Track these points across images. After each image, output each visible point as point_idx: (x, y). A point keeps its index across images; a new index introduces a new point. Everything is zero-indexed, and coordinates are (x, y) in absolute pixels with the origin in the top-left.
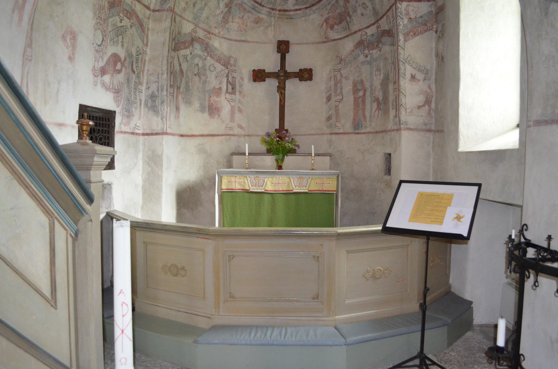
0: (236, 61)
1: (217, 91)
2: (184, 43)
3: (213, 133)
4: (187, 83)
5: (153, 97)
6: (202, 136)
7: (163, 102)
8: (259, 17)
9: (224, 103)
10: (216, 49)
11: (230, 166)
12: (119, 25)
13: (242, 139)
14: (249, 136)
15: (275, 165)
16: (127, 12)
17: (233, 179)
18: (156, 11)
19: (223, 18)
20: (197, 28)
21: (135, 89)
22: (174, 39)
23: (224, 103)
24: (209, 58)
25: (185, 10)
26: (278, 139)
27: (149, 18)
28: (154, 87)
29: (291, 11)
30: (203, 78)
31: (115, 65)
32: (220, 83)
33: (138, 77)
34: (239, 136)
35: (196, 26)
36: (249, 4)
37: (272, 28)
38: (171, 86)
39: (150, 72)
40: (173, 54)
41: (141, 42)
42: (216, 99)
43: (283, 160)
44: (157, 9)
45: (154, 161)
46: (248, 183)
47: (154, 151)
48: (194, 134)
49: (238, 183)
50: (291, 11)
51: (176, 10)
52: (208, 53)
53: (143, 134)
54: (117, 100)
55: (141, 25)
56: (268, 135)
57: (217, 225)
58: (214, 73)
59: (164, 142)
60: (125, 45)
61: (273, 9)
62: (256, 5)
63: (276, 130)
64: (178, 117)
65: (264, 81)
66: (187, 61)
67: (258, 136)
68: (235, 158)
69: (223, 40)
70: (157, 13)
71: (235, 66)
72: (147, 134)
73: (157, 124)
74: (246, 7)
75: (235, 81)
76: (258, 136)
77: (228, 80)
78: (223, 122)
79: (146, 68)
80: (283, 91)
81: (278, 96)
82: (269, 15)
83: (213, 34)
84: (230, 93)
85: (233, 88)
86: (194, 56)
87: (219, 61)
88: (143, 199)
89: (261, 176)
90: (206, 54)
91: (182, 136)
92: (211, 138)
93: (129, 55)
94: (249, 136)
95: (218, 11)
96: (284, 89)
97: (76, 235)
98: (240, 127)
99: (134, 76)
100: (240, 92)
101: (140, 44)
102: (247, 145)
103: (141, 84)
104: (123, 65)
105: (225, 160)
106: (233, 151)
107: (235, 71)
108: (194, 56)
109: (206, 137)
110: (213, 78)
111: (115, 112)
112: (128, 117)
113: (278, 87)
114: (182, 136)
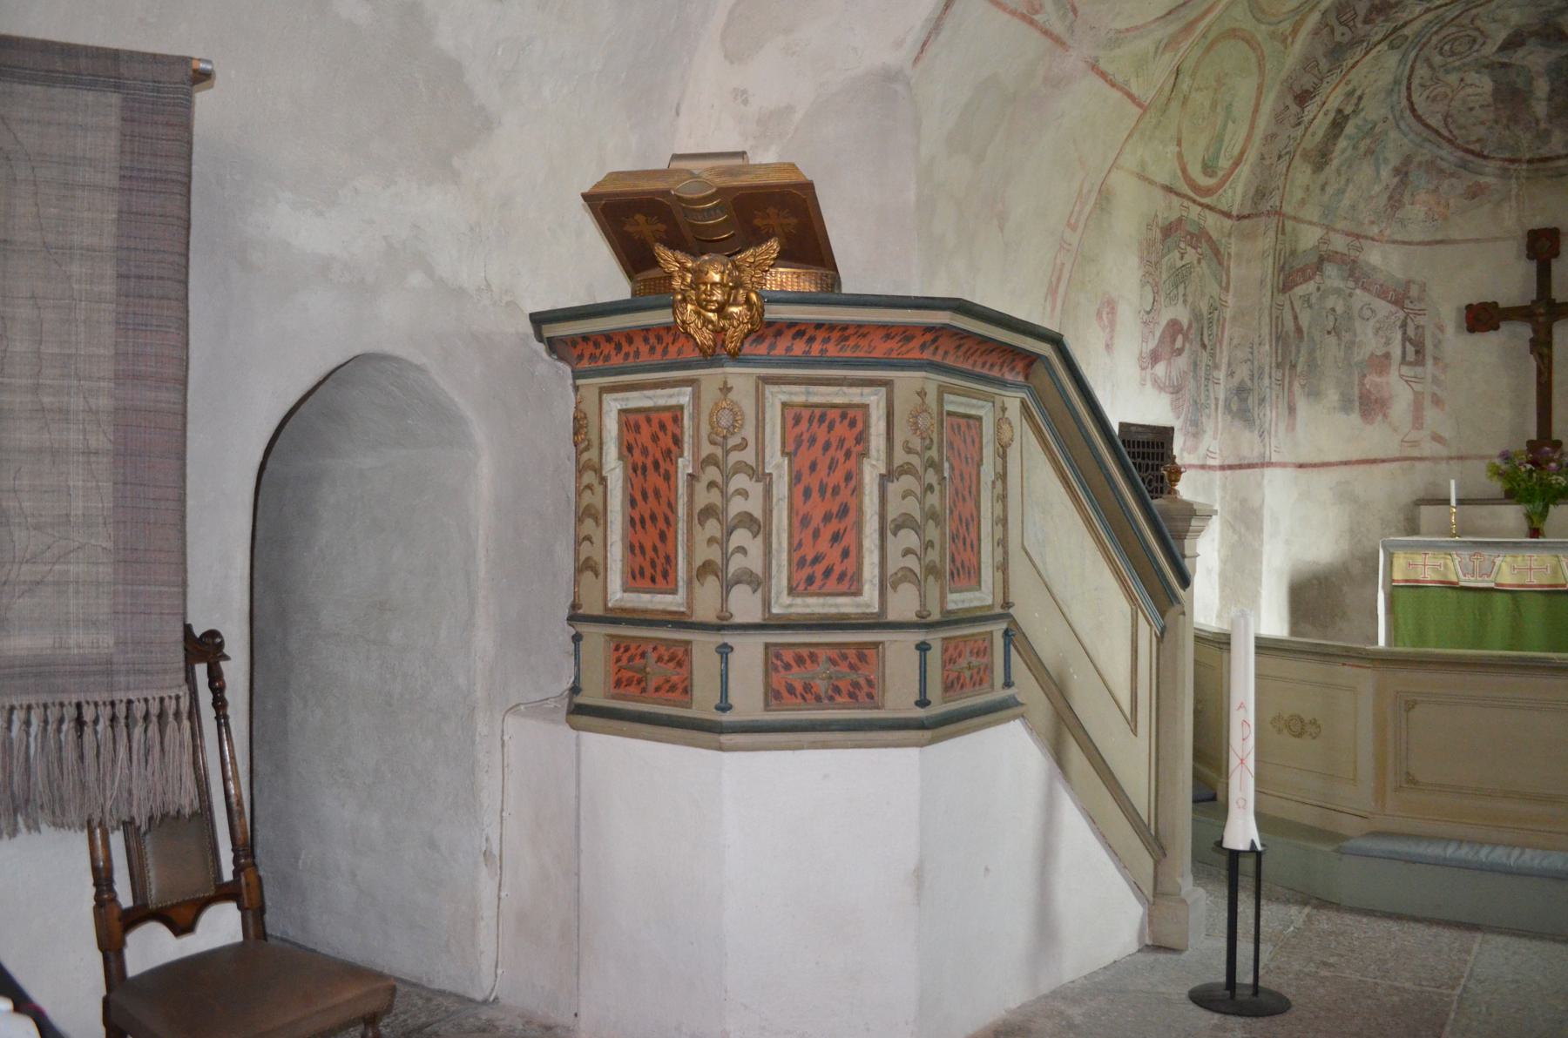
0: (1423, 288)
1: (1381, 363)
2: (1303, 270)
3: (1372, 457)
4: (1311, 352)
5: (1241, 391)
6: (1346, 463)
7: (1262, 401)
8: (1478, 184)
9: (1401, 395)
10: (1374, 268)
11: (1413, 529)
12: (1179, 264)
13: (1443, 466)
14: (1461, 458)
15: (1525, 527)
16: (1192, 235)
17: (1419, 559)
18: (1244, 217)
19: (1390, 198)
20: (1331, 234)
21: (1207, 379)
22: (1282, 268)
23: (1398, 388)
24: (1358, 291)
25: (1303, 202)
26: (1529, 466)
27: (1229, 235)
28: (1243, 372)
29: (1559, 157)
30: (1346, 337)
31: (1174, 341)
32: (1387, 343)
33: (1213, 355)
34: (1434, 459)
35: (1329, 228)
36: (1452, 159)
37: (1514, 203)
38: (1278, 366)
39: (1235, 342)
40: (1281, 298)
41: (1216, 286)
42: (1378, 379)
43: (1544, 514)
44: (1246, 212)
45: (1246, 520)
46: (1456, 567)
47: (1243, 501)
48: (1326, 459)
49: (1429, 567)
50: (1559, 157)
51: (1288, 209)
52: (1356, 281)
53: (1222, 468)
54: (1176, 408)
55: (1217, 252)
56: (1506, 456)
57: (1382, 642)
58: (1372, 322)
59: (1266, 482)
60: (1190, 299)
61: (1512, 161)
62: (1470, 157)
63: (1530, 443)
64: (1293, 429)
65: (1496, 328)
66: (1310, 306)
67: (1482, 457)
68: (1426, 512)
69: (1389, 248)
70: (1246, 222)
71: (1420, 300)
72: (1231, 467)
73: (1249, 445)
74: (1444, 165)
75: (1423, 335)
76: (1482, 457)
77: (1405, 333)
78: (1395, 430)
79: (1226, 335)
80: (1546, 351)
81: (1532, 363)
82: (1504, 174)
83: (1366, 237)
84: (1410, 364)
85: (1417, 350)
86: (1323, 293)
87: (1382, 294)
88: (1222, 598)
89: (1486, 553)
90: (1351, 284)
91: (1301, 466)
92: (1366, 467)
93: (1197, 316)
94: (1461, 458)
95: (1377, 188)
96: (1549, 344)
97: (1162, 633)
98: (1437, 438)
99: (1205, 355)
100: (1436, 359)
101: (1214, 289)
102: (1453, 483)
103: (1216, 367)
104: (1186, 338)
105: (1401, 517)
106: (1421, 494)
107: (1421, 313)
108: (1323, 293)
109: (1355, 467)
110: (1370, 332)
111: (1172, 429)
112: (1195, 435)
113: (1532, 340)
114: (1301, 466)
